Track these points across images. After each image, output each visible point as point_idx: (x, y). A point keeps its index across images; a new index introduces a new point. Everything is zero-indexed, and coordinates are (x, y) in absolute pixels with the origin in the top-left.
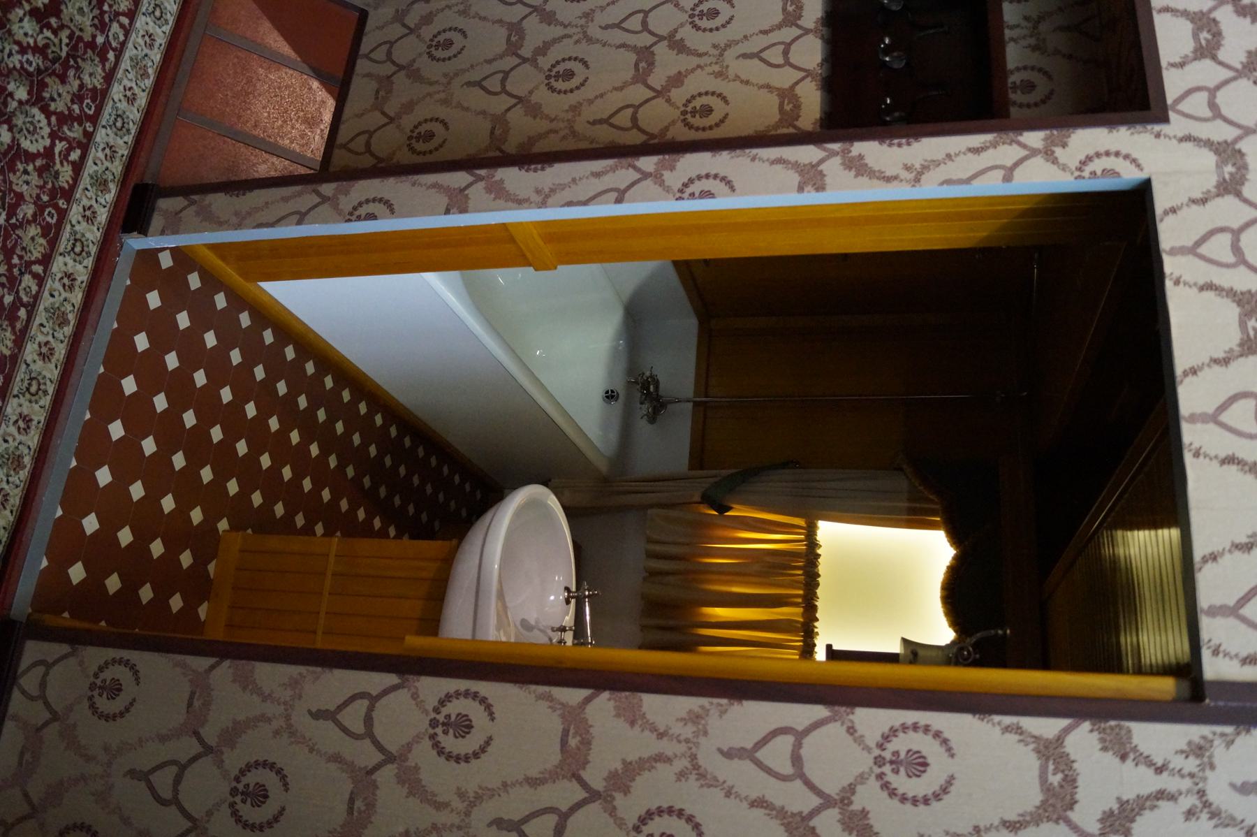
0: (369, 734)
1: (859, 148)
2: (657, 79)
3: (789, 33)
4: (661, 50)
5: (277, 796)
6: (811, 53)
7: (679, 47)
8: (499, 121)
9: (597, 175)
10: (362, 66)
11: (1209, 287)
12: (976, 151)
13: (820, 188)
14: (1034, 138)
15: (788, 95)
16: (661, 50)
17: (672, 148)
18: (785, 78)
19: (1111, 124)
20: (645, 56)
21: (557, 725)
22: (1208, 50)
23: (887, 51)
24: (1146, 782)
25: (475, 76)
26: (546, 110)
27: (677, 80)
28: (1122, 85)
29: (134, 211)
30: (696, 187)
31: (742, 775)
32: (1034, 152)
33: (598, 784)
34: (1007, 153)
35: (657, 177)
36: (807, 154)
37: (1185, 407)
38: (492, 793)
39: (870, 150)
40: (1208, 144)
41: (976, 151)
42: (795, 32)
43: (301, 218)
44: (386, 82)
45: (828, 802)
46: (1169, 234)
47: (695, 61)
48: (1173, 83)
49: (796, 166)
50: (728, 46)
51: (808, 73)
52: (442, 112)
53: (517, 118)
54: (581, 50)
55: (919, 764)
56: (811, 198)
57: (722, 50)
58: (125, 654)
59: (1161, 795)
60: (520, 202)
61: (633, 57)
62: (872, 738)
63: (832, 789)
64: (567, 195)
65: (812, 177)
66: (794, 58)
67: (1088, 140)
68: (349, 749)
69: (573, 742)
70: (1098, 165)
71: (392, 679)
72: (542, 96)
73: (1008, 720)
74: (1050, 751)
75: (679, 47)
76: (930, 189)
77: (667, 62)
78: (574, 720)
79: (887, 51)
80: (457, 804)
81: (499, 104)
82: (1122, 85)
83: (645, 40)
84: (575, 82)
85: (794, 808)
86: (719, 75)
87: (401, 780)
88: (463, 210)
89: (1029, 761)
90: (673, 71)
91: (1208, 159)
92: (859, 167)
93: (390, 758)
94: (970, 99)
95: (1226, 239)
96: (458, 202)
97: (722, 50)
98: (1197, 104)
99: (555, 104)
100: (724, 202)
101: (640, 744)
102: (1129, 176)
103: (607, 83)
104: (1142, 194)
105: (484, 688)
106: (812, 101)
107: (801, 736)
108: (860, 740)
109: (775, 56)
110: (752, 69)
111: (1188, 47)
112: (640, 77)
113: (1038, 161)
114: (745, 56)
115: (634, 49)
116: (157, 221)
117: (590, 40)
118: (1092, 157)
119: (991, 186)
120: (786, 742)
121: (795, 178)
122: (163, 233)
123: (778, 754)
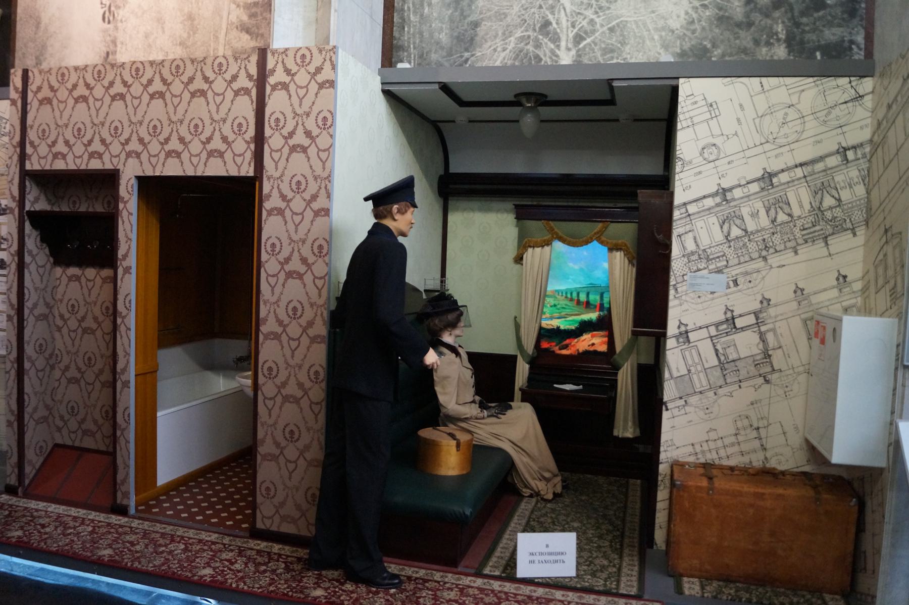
0: (280, 150)
1: (120, 256)
2: (94, 326)
3: (83, 280)
4: (84, 427)
5: (292, 427)
6: (91, 272)
7: (83, 420)
8: (103, 385)
9: (121, 337)
10: (77, 444)
11: (163, 164)
12: (123, 222)
13: (130, 268)
14: (121, 206)
15: (104, 280)
16: (84, 427)
17: (115, 425)
18: (99, 281)
19: (118, 184)
20: (85, 331)
21: (266, 462)
22: (100, 156)
23: (92, 247)
24: (280, 66)
25: (86, 395)
26: (101, 367)
27: (95, 319)
28: (110, 178)
29: (122, 511)
30: (128, 305)
31: (281, 165)
32: (123, 321)
33: (279, 451)
34: (125, 214)
35: (124, 317)
36: (120, 271)
37: (193, 174)
38: (286, 360)
39: (121, 253)
40: (126, 159)
41: (123, 222)
42: (83, 277)
43: (128, 442)
44: (86, 432)
45: (286, 142)
46: (149, 173)
47: (89, 312)
48: (109, 166)
49: (124, 275)
50: (85, 300)
51: (98, 273)
52: (98, 409)
53: (103, 378)
54: (81, 354)
55: (277, 120)
56: (134, 271)
57: (87, 303)
58: (258, 486)
59: (278, 188)
60: (128, 474)
61: (86, 335)
62: (272, 132)
63: (280, 267)
64: (129, 232)
65: (127, 270)
66: (92, 278)
67: (122, 192)
68: (278, 404)
69: (270, 458)
70: (130, 189)
71: (262, 270)
72: (96, 369)
73: (267, 98)
74: (274, 88)
75: (83, 420)
76: (134, 236)
77: (89, 323)
78: (266, 337)
79: (92, 247)
80: (292, 245)
81: (98, 385)
82: (110, 178)
83: (80, 433)
84: (93, 357)
85: (284, 277)
86: (95, 304)
87: (284, 387)
88: (129, 382)
89: (272, 218)
90: (92, 320)
91: (130, 160)
92: (125, 256)
93: (279, 391)
94: (108, 223)
95: (152, 159)
96: (126, 384)
97: (87, 303)
98: (115, 161)
99: (99, 365)
100: (133, 297)
101: (269, 440)
102: (134, 181)
103: (92, 345)
104: (139, 178)
105: (263, 241)
106: (107, 272)
107: (268, 275)
108: (269, 260)
109: (90, 388)
110: (95, 292)
111: (99, 161)
112: (93, 332)
113: (128, 205)
114: (89, 295)
115: (83, 334)
116: (125, 502)
117: (78, 351)
118: (128, 191)
119: (134, 219)
120: (270, 278)
121: (127, 275)
122: (129, 498)
123: (270, 403)
